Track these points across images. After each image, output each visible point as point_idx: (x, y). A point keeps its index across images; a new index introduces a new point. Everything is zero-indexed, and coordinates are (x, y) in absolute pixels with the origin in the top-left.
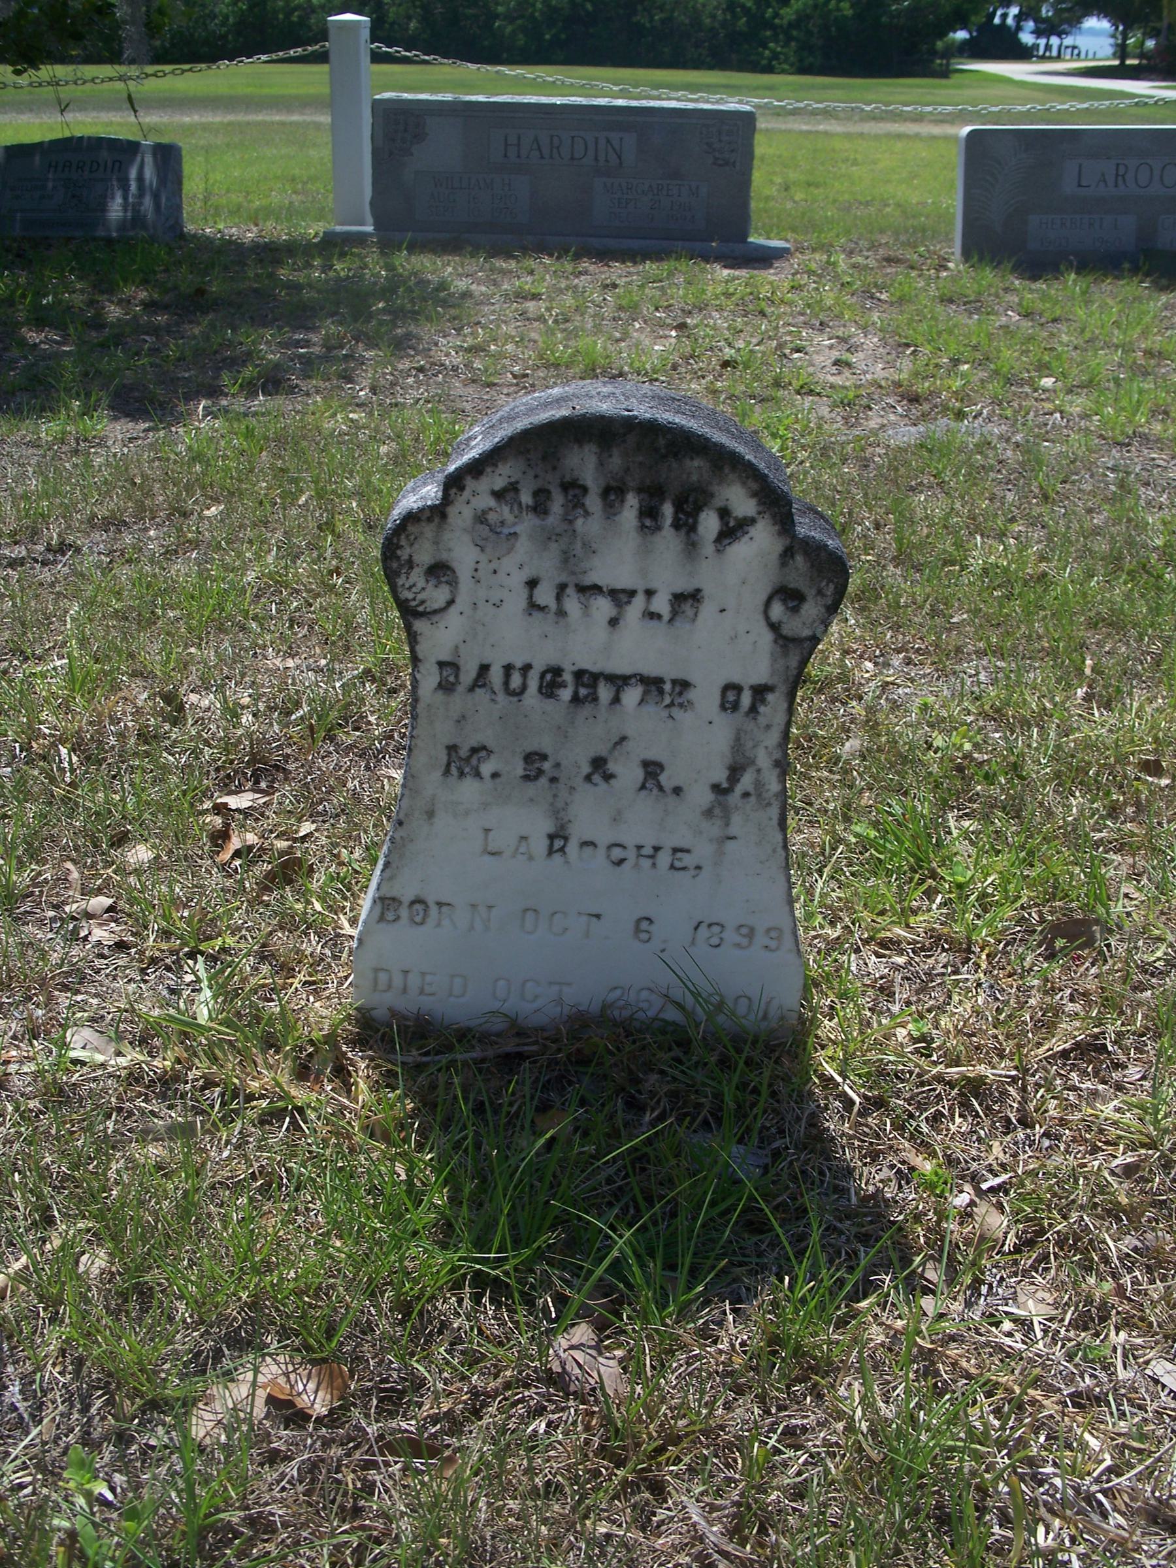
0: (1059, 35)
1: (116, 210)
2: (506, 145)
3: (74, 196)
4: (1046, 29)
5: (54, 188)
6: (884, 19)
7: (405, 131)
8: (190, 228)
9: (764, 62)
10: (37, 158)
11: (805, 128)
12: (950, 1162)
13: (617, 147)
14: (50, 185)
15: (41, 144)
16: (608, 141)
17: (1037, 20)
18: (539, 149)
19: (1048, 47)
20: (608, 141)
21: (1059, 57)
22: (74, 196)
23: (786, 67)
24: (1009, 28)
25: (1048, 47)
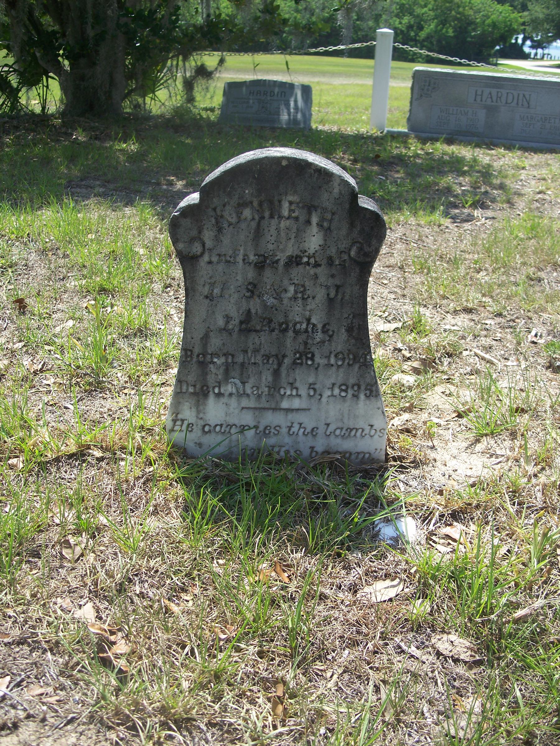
0: (542, 48)
1: (285, 117)
2: (476, 95)
3: (263, 107)
4: (537, 45)
5: (253, 103)
6: (469, 39)
7: (429, 85)
8: (314, 126)
9: (410, 57)
10: (244, 89)
11: (345, 82)
12: (165, 362)
13: (528, 99)
14: (251, 101)
15: (245, 82)
16: (524, 96)
17: (532, 41)
18: (491, 98)
19: (536, 54)
20: (524, 96)
21: (542, 58)
22: (263, 107)
23: (420, 60)
24: (518, 44)
25: (536, 54)
